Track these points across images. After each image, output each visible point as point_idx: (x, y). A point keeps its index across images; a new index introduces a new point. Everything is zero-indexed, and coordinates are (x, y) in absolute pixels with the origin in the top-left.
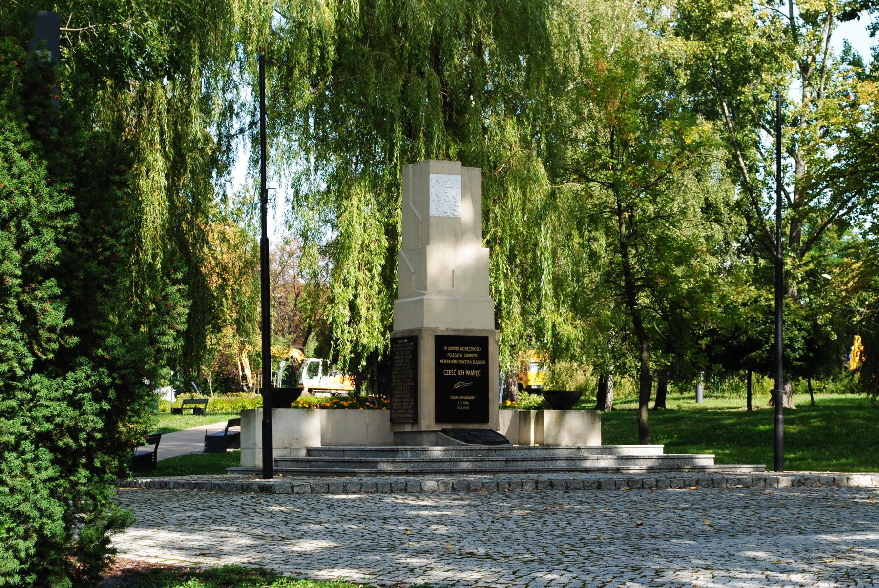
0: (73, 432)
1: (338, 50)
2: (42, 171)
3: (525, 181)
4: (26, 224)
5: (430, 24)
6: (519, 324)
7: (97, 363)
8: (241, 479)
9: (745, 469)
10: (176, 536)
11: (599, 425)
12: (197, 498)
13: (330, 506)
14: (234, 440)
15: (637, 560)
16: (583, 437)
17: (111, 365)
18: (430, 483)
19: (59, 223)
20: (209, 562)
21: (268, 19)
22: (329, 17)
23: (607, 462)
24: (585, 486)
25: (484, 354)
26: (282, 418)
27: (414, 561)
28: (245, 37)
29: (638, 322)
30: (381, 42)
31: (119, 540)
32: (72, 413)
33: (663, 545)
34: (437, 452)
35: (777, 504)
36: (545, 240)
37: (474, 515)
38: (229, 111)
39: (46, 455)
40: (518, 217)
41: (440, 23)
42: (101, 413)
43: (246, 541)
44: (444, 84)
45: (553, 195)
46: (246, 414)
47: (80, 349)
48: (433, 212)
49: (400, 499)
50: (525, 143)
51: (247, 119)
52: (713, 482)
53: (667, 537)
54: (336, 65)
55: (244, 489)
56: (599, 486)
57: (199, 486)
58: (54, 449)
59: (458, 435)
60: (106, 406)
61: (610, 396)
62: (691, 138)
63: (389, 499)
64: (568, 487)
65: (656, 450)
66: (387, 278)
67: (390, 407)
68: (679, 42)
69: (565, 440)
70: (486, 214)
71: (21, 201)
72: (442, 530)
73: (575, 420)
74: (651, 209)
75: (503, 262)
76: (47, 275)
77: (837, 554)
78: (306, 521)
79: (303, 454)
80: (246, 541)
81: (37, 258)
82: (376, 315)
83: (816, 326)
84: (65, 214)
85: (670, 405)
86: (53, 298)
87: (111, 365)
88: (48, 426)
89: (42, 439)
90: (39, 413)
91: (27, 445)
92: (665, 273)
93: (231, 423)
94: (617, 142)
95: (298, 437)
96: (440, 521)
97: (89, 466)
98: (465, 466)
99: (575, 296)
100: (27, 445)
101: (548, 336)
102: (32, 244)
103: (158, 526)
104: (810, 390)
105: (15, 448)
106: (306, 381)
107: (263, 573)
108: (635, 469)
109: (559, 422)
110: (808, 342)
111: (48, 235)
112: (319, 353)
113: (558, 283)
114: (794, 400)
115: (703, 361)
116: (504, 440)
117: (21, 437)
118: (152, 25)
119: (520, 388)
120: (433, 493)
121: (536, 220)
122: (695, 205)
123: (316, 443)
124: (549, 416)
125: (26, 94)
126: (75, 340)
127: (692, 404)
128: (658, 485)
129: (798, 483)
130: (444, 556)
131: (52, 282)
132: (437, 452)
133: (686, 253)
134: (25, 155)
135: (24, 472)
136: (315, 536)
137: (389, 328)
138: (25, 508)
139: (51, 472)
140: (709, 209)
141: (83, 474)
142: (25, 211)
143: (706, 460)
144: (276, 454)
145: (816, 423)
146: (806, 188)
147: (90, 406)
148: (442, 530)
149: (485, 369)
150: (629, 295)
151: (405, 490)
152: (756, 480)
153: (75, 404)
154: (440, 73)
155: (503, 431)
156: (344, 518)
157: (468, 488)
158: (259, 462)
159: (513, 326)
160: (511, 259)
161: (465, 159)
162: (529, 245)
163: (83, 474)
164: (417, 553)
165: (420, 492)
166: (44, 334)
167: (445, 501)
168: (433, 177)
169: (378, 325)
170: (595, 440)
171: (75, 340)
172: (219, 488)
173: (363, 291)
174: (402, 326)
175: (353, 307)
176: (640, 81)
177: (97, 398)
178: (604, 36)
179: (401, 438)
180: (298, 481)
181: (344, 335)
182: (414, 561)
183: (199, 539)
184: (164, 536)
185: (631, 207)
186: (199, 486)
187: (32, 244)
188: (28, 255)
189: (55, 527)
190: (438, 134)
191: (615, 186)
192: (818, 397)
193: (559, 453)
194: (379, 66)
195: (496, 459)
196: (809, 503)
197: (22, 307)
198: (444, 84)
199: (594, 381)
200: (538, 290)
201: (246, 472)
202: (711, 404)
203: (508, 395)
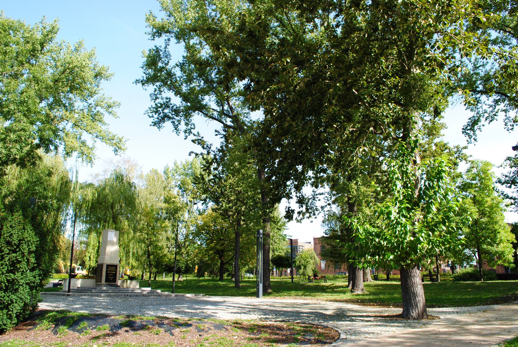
0: (34, 283)
1: (92, 205)
2: (34, 233)
3: (128, 234)
4: (30, 243)
5: (111, 201)
6: (124, 262)
7: (40, 270)
8: (63, 293)
9: (166, 293)
10: (50, 304)
11: (139, 284)
12: (54, 297)
13: (82, 299)
14: (60, 284)
15: (141, 310)
16: (135, 286)
17: (43, 270)
18: (103, 295)
19: (36, 243)
20: (57, 309)
21: (78, 197)
22: (91, 197)
23: (139, 291)
24: (134, 296)
25: (116, 269)
26: (73, 280)
27: (98, 309)
28: (73, 201)
29: (150, 262)
30: (101, 204)
31: (39, 304)
32: (34, 279)
33: (146, 307)
34: (105, 288)
35: (170, 300)
36: (131, 245)
37: (111, 301)
38: (67, 215)
39: (28, 287)
40: (126, 241)
41: (113, 200)
42: (40, 279)
43: (64, 305)
44: (113, 213)
45: (134, 237)
46: (64, 279)
47: (37, 267)
48: (108, 239)
49: (96, 298)
50: (129, 226)
51: (71, 216)
52: (160, 295)
53: (147, 305)
54: (91, 208)
55: (64, 295)
56: (137, 296)
57: (54, 294)
58: (29, 286)
59: (109, 285)
60: (41, 278)
61: (144, 277)
62: (163, 225)
63: (94, 298)
64: (131, 296)
65: (149, 289)
66: (98, 251)
67: (96, 279)
68: (164, 204)
69: (132, 287)
70: (119, 240)
71: (29, 239)
72: (104, 304)
73: (134, 282)
74: (155, 239)
75: (122, 249)
76: (32, 253)
77: (178, 308)
78: (77, 302)
79: (76, 288)
80: (64, 305)
81: (31, 250)
82: (94, 259)
83: (187, 264)
84: (37, 241)
85: (157, 279)
86: (33, 257)
87: (43, 270)
88: (29, 281)
89: (27, 284)
90: (27, 279)
91: (24, 285)
92: (156, 252)
93: (60, 281)
94: (148, 225)
95: (76, 285)
96: (104, 302)
97: (36, 289)
98: (110, 291)
99: (137, 257)
100: (24, 285)
101: (130, 265)
102: (30, 247)
103: (46, 302)
104: (186, 277)
105: (22, 285)
106: (77, 272)
107: (68, 311)
108: (145, 293)
109: (131, 283)
110: (186, 267)
111: (34, 245)
112: (80, 265)
113: (133, 254)
114: (182, 279)
115: (163, 271)
116: (119, 286)
117: (23, 283)
118: (55, 201)
119: (125, 274)
120: (103, 297)
121: (129, 242)
122: (165, 238)
123: (79, 286)
124: (129, 281)
125: (32, 219)
126: (36, 265)
127: (162, 279)
128: (148, 296)
129: (176, 296)
130: (104, 308)
131: (33, 254)
132: (105, 288)
133: (161, 248)
134: (31, 230)
135: (23, 290)
136: (79, 304)
137: (97, 262)
138: (23, 297)
139: (28, 290)
140: (168, 239)
141: (34, 291)
142: (30, 241)
143: (159, 291)
144: (71, 288)
145: (185, 284)
146: (187, 236)
147: (38, 278)
148: (104, 304)
149: (116, 272)
150: (149, 257)
151: (97, 296)
152: (168, 295)
153: (35, 277)
154: (112, 210)
155: (119, 284)
156: (85, 301)
157: (110, 296)
158: (67, 289)
159: (123, 263)
160: (124, 249)
161: (116, 229)
162: (128, 246)
163: (34, 291)
164: (99, 308)
165: (100, 296)
166: (30, 264)
167: (105, 298)
168: (109, 233)
169: (95, 262)
170: (138, 287)
171: (36, 265)
172: (58, 295)
173: (92, 254)
174: (100, 262)
175: (90, 257)
176: (155, 213)
177: (39, 276)
178: (147, 202)
179: (97, 285)
180: (75, 294)
181: (87, 263)
182: (98, 309)
183: (54, 305)
184: (47, 304)
185: (150, 239)
186: (54, 294)
187: (30, 247)
188: (29, 249)
189: (28, 301)
190: (110, 222)
191: (147, 234)
192: (188, 278)
193: (130, 289)
194: (100, 208)
195: (117, 290)
196: (176, 300)
197: (27, 259)
198: (113, 213)
199: (141, 274)
200: (129, 256)
201: (64, 291)
202: (165, 279)
203: (122, 277)
